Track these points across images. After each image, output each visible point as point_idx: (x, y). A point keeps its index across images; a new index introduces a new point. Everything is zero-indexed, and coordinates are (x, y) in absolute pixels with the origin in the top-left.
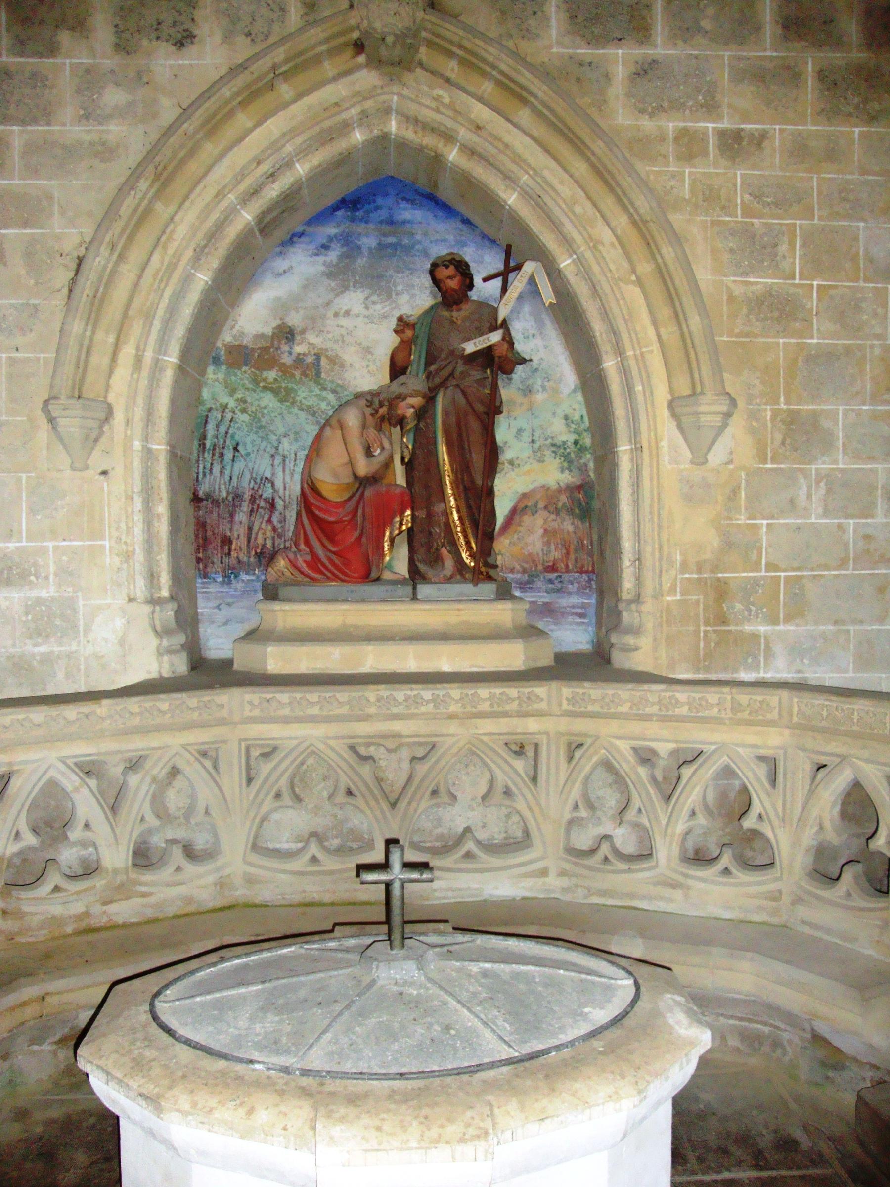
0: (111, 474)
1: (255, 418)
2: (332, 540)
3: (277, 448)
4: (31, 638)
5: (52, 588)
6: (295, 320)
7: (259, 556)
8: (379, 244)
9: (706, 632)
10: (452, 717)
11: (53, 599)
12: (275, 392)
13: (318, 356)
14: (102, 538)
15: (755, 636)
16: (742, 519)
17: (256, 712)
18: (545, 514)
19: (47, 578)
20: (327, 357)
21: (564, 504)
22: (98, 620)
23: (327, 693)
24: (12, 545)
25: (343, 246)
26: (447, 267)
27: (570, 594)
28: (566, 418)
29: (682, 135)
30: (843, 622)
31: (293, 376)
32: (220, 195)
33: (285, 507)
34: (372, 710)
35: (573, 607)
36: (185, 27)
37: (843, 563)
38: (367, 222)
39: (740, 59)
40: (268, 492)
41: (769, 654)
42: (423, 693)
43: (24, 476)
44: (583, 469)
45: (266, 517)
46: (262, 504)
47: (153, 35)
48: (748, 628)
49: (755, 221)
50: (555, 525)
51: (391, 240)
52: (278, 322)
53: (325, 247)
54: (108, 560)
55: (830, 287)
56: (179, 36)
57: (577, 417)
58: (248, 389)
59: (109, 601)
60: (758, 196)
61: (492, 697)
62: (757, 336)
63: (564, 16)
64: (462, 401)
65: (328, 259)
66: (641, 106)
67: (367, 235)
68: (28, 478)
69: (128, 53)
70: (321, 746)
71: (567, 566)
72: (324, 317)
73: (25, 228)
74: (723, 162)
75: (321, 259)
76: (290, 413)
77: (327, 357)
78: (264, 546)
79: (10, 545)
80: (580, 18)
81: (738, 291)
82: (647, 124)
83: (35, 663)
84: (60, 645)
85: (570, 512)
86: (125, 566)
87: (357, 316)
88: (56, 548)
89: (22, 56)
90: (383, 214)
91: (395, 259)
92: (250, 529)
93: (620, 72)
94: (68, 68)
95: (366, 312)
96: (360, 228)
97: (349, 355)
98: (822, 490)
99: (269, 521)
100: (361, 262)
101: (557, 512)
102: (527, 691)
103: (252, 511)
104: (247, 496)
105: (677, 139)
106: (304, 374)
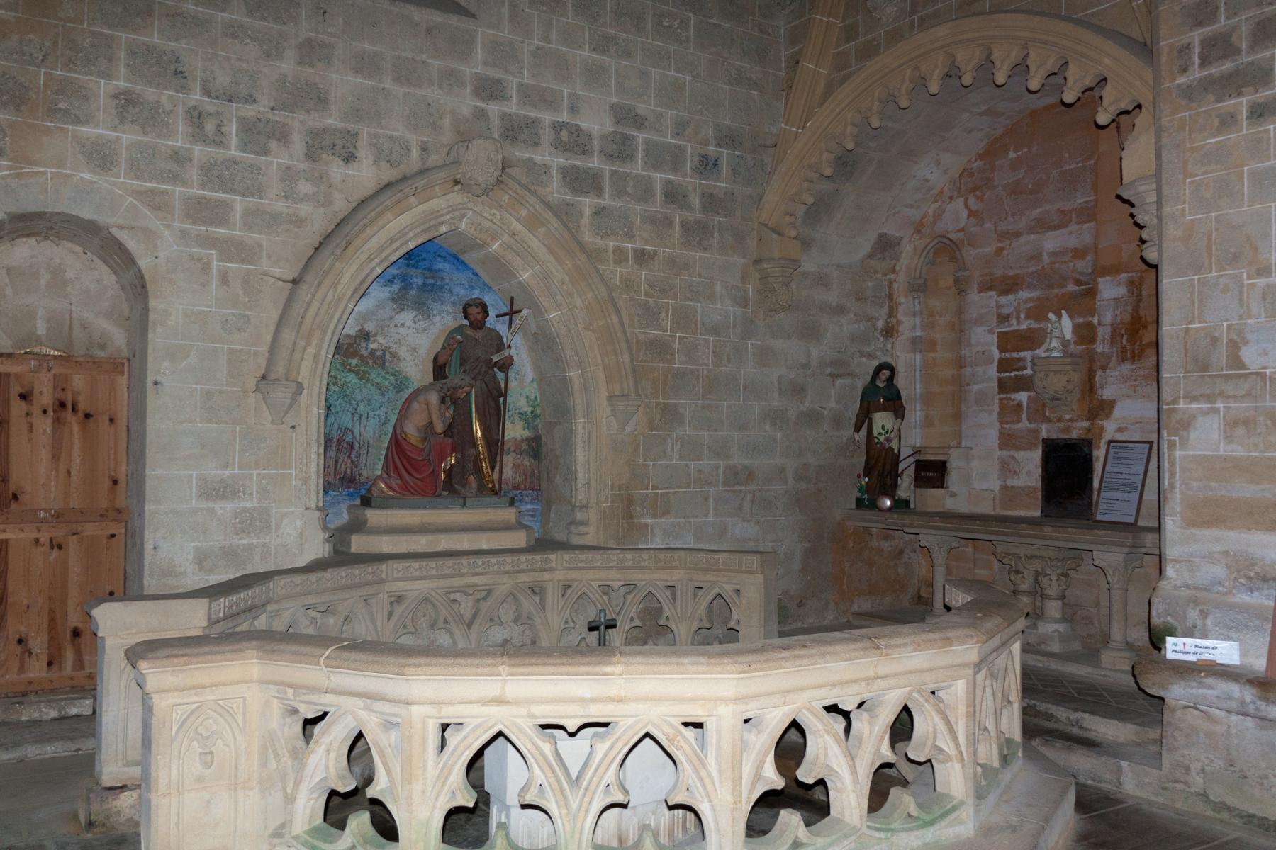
0: (297, 428)
1: (343, 389)
2: (418, 471)
3: (356, 409)
4: (237, 534)
5: (255, 501)
6: (370, 327)
7: (342, 479)
8: (1004, 488)
9: (622, 523)
10: (507, 572)
11: (255, 509)
12: (357, 373)
13: (384, 352)
14: (290, 468)
15: (646, 525)
16: (640, 461)
17: (400, 575)
18: (514, 454)
19: (251, 494)
20: (390, 352)
21: (524, 450)
22: (285, 521)
23: (440, 562)
24: (227, 473)
25: (401, 282)
26: (477, 307)
27: (527, 503)
28: (527, 397)
29: (617, 250)
30: (688, 517)
31: (368, 363)
32: (370, 259)
33: (360, 448)
34: (464, 571)
35: (529, 511)
36: (350, 150)
37: (688, 486)
38: (416, 268)
39: (645, 210)
40: (349, 438)
41: (653, 535)
42: (492, 560)
43: (238, 427)
44: (536, 428)
45: (348, 454)
46: (345, 445)
47: (330, 152)
48: (643, 521)
49: (650, 299)
50: (519, 461)
51: (431, 281)
52: (360, 328)
53: (391, 282)
54: (294, 483)
55: (684, 337)
56: (346, 155)
57: (533, 397)
58: (338, 370)
59: (293, 509)
60: (652, 286)
61: (527, 561)
62: (649, 362)
63: (560, 176)
64: (484, 385)
65: (392, 289)
66: (597, 231)
67: (416, 276)
68: (241, 428)
69: (314, 161)
70: (433, 594)
71: (525, 486)
72: (388, 326)
73: (243, 264)
74: (636, 266)
75: (388, 289)
76: (365, 387)
77: (390, 352)
78: (345, 472)
79: (226, 472)
80: (568, 179)
81: (641, 337)
82: (600, 242)
83: (239, 551)
84: (258, 538)
85: (528, 454)
86: (304, 487)
87: (409, 328)
88: (259, 475)
89: (245, 152)
90: (426, 264)
91: (433, 293)
92: (336, 461)
93: (587, 211)
94: (275, 164)
95: (415, 326)
96: (412, 271)
97: (403, 352)
98: (679, 446)
99: (349, 456)
100: (412, 293)
101: (521, 454)
102: (545, 556)
103: (338, 450)
104: (335, 440)
105: (614, 251)
106: (375, 362)
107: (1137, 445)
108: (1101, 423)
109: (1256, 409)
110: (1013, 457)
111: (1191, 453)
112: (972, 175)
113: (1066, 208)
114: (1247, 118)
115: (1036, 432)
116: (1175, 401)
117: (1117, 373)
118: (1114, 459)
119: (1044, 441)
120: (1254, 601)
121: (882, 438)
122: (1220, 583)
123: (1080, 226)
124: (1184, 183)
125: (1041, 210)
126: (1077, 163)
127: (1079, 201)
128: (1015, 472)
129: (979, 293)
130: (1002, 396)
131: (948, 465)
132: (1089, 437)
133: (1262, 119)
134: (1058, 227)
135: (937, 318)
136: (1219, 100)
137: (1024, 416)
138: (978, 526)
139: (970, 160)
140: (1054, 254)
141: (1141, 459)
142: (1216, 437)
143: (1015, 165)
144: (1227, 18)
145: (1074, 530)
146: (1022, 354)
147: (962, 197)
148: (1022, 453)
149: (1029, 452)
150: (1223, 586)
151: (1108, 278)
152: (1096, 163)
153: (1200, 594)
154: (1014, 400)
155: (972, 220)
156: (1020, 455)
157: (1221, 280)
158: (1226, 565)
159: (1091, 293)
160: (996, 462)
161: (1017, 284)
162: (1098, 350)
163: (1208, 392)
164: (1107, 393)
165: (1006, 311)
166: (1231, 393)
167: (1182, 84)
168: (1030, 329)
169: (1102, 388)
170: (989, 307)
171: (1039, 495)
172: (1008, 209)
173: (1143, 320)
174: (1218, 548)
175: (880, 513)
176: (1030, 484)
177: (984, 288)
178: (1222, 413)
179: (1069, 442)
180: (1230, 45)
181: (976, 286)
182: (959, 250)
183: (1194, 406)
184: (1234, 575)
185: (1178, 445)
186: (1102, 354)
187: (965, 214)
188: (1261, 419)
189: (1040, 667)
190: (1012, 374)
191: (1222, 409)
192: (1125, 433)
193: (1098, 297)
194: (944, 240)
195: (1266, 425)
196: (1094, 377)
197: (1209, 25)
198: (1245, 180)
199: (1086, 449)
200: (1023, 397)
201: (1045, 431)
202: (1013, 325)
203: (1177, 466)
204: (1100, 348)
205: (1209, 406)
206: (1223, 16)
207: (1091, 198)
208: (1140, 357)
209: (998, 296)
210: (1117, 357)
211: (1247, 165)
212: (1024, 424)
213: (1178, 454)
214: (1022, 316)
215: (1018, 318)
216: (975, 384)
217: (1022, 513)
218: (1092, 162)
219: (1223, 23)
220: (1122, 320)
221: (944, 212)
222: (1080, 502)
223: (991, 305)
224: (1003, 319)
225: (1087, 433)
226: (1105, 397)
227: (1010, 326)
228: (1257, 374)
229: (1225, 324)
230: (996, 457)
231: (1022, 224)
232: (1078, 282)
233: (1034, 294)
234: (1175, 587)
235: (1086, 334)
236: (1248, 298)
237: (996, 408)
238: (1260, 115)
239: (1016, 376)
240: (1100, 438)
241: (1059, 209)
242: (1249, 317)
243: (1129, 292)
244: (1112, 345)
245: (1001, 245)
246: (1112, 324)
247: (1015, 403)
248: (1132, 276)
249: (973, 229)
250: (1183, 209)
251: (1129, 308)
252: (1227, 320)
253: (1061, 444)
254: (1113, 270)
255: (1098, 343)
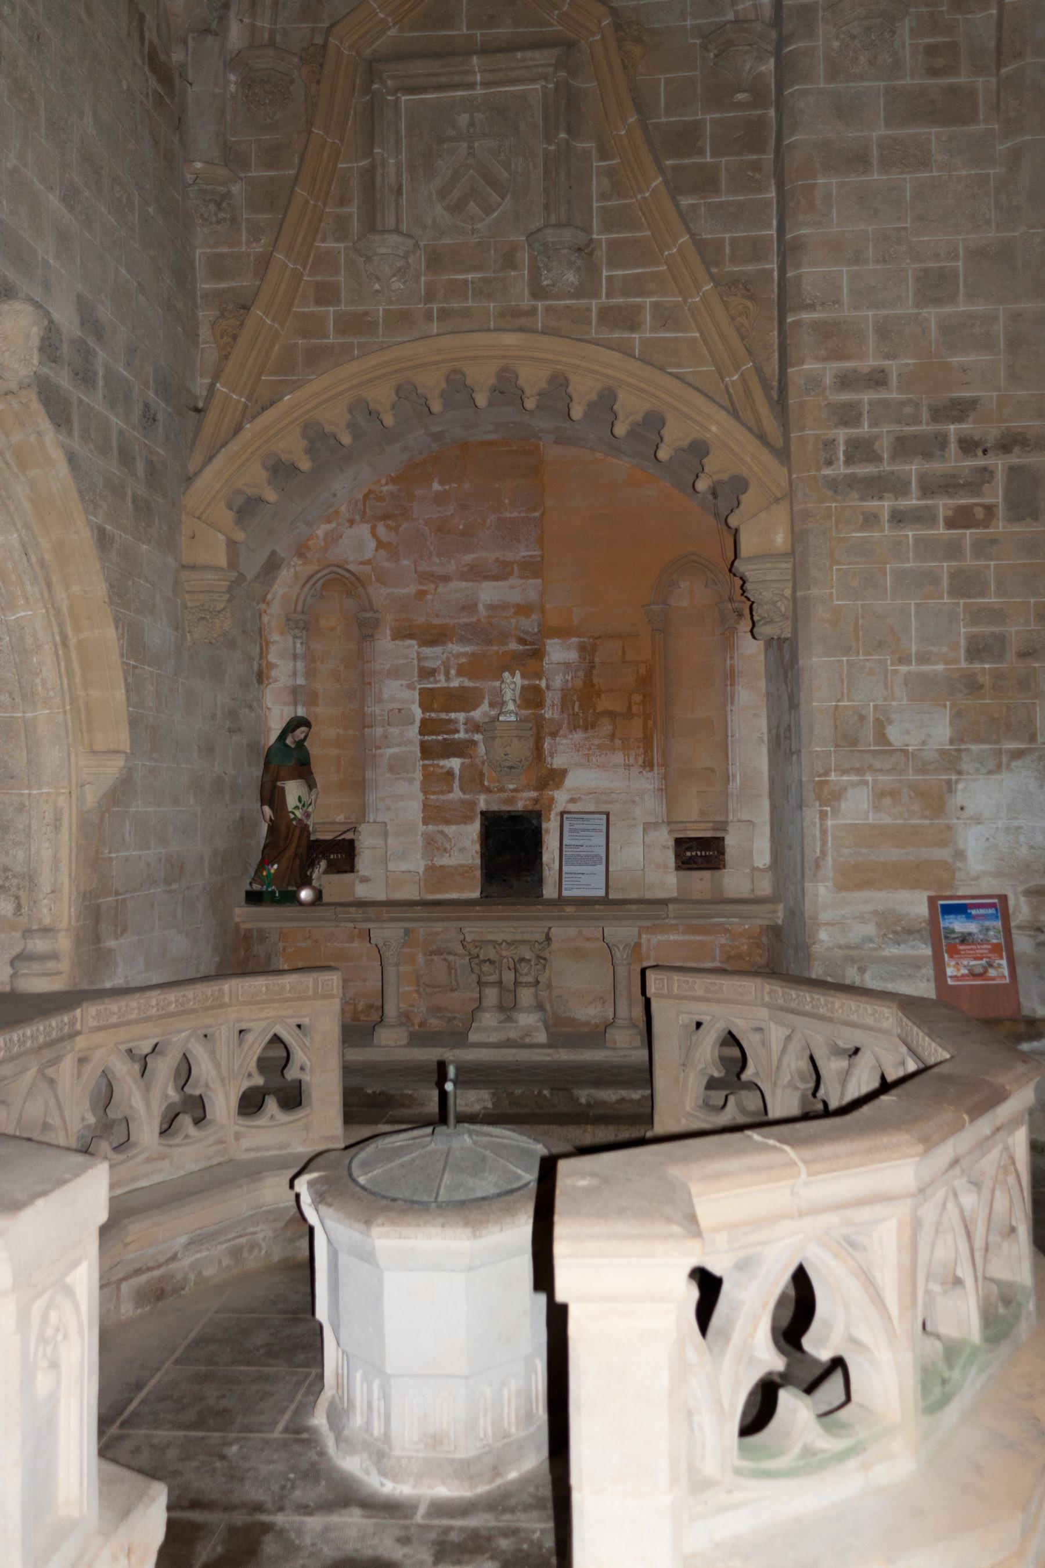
8: (430, 869)
107: (592, 816)
108: (551, 793)
109: (900, 781)
110: (442, 833)
111: (842, 822)
112: (380, 499)
113: (507, 559)
114: (889, 521)
115: (472, 804)
116: (827, 773)
117: (569, 741)
118: (571, 831)
119: (482, 813)
120: (902, 952)
121: (299, 814)
122: (871, 940)
123: (523, 581)
124: (831, 569)
125: (475, 556)
126: (519, 512)
127: (522, 554)
128: (445, 850)
129: (394, 640)
130: (427, 762)
131: (356, 844)
132: (537, 808)
133: (902, 525)
134: (497, 578)
135: (319, 663)
136: (863, 499)
137: (456, 785)
138: (477, 912)
139: (379, 481)
140: (492, 607)
141: (601, 831)
142: (865, 807)
143: (440, 499)
144: (870, 426)
145: (602, 907)
146: (453, 715)
147: (368, 522)
148: (454, 828)
149: (462, 825)
150: (874, 942)
151: (556, 640)
152: (542, 515)
153: (853, 953)
154: (442, 767)
155: (382, 553)
156: (451, 830)
157: (867, 664)
158: (876, 923)
159: (538, 654)
160: (419, 838)
161: (445, 635)
162: (547, 716)
163: (858, 765)
164: (558, 762)
165: (430, 664)
166: (879, 767)
167: (828, 475)
168: (463, 687)
169: (552, 756)
170: (407, 658)
171: (478, 873)
172: (432, 548)
173: (597, 687)
174: (869, 908)
175: (301, 908)
176: (464, 862)
177: (402, 633)
178: (870, 785)
179: (513, 814)
180: (873, 451)
181: (388, 632)
182: (364, 587)
183: (845, 778)
184: (883, 932)
185: (829, 814)
186: (552, 720)
187: (372, 544)
188: (905, 790)
189: (549, 1061)
190: (440, 738)
191: (870, 782)
192: (578, 804)
193: (546, 660)
194: (340, 571)
195: (910, 796)
196: (542, 746)
197: (853, 427)
198: (888, 576)
199: (535, 822)
200: (455, 763)
201: (483, 803)
202: (439, 681)
203: (829, 834)
204: (548, 714)
205: (859, 778)
206: (866, 422)
207: (536, 553)
208: (593, 726)
209: (420, 646)
210: (569, 724)
211: (890, 563)
212: (457, 794)
213: (829, 823)
214: (453, 672)
215: (447, 674)
216: (389, 747)
217: (454, 896)
218: (537, 514)
219: (866, 430)
220: (573, 686)
221: (341, 537)
222: (529, 879)
223: (411, 657)
224: (427, 673)
225: (534, 805)
226: (555, 766)
227: (436, 682)
228: (901, 750)
229: (872, 704)
230: (420, 833)
231: (452, 568)
232: (522, 641)
233: (468, 649)
234: (828, 949)
235: (533, 698)
236: (892, 682)
237: (418, 775)
238: (900, 521)
239: (445, 739)
240: (550, 808)
241: (497, 559)
242: (893, 699)
243: (580, 658)
244: (562, 712)
245: (424, 588)
246: (562, 690)
247: (444, 770)
248: (584, 642)
249: (386, 564)
250: (831, 593)
251: (581, 674)
252: (873, 701)
253: (506, 816)
254: (562, 632)
255: (547, 708)
